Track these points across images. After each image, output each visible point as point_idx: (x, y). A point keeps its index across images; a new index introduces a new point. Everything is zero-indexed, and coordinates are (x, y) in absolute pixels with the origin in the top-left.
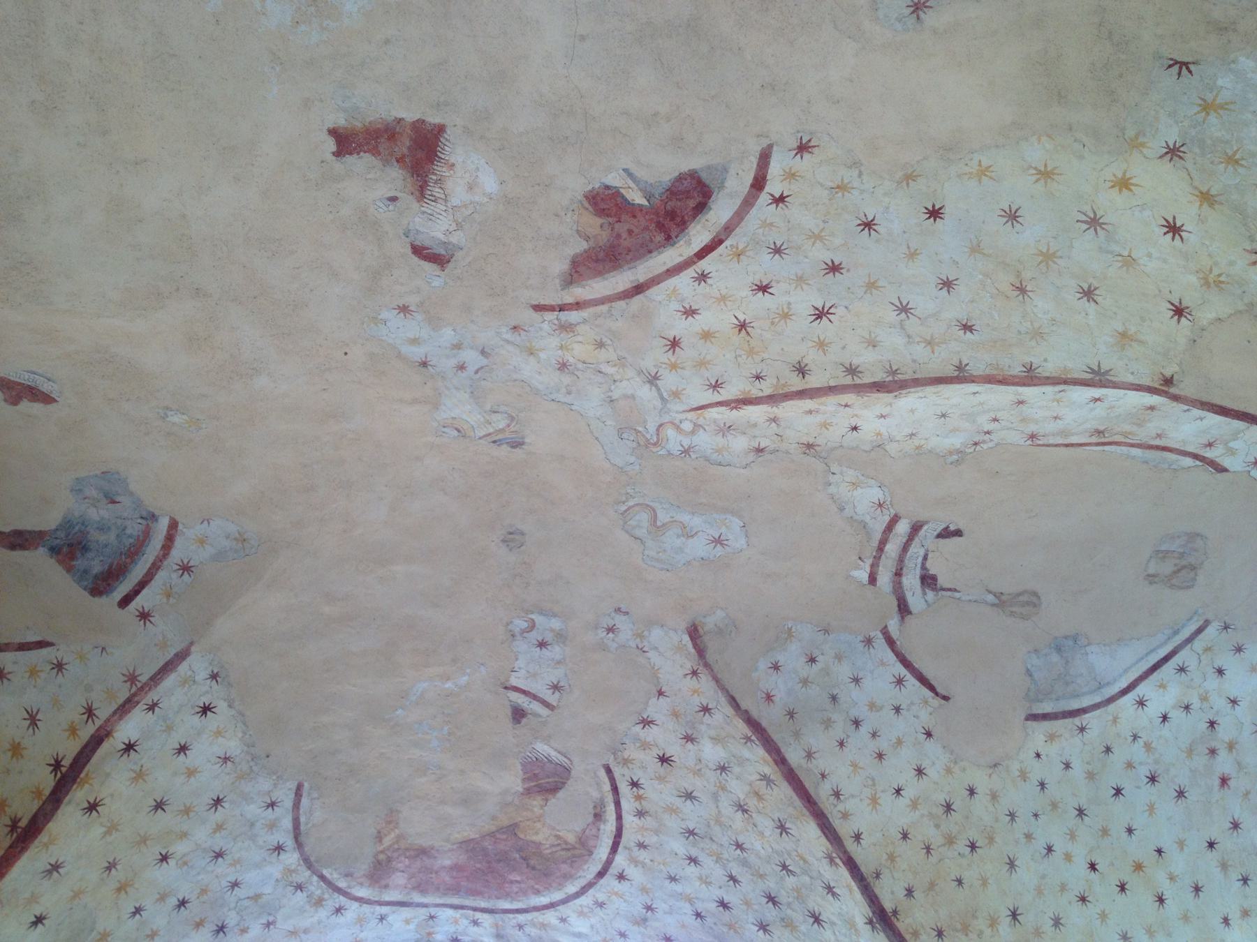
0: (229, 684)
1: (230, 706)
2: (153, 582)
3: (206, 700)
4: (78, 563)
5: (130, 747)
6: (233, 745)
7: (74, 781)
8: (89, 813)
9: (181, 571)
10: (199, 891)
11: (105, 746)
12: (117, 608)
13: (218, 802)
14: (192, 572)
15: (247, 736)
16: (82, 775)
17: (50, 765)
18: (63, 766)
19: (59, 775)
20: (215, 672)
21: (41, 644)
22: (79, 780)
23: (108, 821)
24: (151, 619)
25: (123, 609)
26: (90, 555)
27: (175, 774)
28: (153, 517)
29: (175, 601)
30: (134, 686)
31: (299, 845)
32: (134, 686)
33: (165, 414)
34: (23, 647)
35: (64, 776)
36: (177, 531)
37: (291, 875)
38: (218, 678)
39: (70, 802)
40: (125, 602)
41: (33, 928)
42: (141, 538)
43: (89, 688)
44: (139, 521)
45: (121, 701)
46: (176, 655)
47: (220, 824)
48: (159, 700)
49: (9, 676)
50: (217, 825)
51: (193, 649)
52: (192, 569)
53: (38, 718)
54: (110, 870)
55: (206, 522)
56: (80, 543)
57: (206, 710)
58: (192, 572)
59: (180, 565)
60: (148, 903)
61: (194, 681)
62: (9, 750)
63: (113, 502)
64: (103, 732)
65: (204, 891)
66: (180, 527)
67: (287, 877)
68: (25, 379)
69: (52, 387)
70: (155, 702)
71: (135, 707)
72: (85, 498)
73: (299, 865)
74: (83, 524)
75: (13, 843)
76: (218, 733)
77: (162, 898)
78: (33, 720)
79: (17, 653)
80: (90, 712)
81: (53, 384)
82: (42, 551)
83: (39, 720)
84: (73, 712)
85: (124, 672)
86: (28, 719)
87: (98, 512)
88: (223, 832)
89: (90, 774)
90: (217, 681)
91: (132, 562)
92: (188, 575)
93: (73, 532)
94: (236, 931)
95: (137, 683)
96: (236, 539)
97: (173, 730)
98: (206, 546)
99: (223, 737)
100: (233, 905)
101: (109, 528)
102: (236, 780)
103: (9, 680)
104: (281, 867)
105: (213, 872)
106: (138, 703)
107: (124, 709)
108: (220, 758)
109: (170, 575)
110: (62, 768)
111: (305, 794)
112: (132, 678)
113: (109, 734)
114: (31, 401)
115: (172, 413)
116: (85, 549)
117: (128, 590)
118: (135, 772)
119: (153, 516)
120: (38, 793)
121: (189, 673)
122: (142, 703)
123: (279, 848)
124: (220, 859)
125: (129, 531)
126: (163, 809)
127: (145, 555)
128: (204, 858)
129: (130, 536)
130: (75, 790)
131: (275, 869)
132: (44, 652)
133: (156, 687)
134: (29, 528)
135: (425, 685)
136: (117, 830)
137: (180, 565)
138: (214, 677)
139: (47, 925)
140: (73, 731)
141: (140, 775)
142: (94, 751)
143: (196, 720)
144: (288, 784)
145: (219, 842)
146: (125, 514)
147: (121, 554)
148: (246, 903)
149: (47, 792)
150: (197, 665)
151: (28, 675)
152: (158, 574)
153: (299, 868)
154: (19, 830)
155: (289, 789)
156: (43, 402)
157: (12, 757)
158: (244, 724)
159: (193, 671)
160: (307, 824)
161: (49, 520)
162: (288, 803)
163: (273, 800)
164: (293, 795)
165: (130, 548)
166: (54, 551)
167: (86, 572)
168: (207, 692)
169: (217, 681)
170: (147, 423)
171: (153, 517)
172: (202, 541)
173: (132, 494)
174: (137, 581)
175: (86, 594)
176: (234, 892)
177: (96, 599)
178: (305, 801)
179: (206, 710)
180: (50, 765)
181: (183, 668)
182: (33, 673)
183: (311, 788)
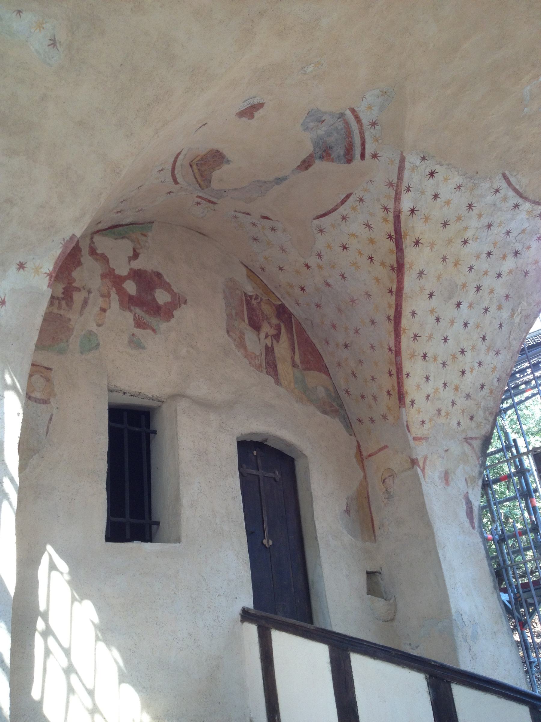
0: (433, 157)
1: (441, 165)
2: (366, 140)
3: (428, 170)
4: (333, 155)
5: (413, 211)
6: (458, 180)
7: (401, 238)
8: (417, 246)
9: (373, 127)
10: (492, 245)
11: (403, 217)
12: (363, 161)
13: (470, 206)
14: (377, 123)
15: (460, 172)
16: (403, 234)
17: (388, 238)
18: (392, 236)
19: (394, 240)
20: (422, 156)
21: (348, 196)
22: (403, 237)
23: (428, 243)
24: (378, 155)
25: (364, 160)
26: (335, 149)
27: (441, 208)
28: (342, 115)
29: (381, 140)
30: (394, 187)
31: (526, 199)
32: (394, 187)
33: (304, 71)
34: (343, 202)
35: (396, 239)
36: (356, 112)
37: (532, 213)
38: (426, 158)
39: (406, 247)
40: (363, 156)
41: (431, 299)
42: (346, 126)
43: (378, 200)
44: (339, 120)
45: (394, 196)
46: (400, 162)
47: (479, 214)
48: (408, 185)
49: (347, 216)
50: (478, 215)
51: (404, 154)
52: (377, 122)
53: (369, 224)
54: (445, 260)
55: (364, 99)
56: (327, 147)
57: (432, 174)
58: (377, 123)
59: (370, 125)
60: (473, 262)
61: (417, 167)
62: (369, 243)
63: (323, 122)
64: (397, 213)
65: (495, 244)
66: (356, 109)
67: (531, 214)
68: (246, 105)
69: (257, 99)
70: (407, 187)
71: (401, 194)
72: (312, 129)
73: (533, 206)
74: (321, 139)
75: (397, 274)
76: (446, 180)
77: (478, 257)
78: (368, 226)
79: (343, 206)
80: (386, 209)
81: (257, 98)
82: (317, 162)
83: (371, 225)
84: (381, 213)
85: (386, 184)
86: (367, 227)
87: (322, 130)
88: (484, 216)
89: (405, 231)
90: (426, 160)
91: (352, 139)
92: (377, 126)
93: (321, 145)
94: (524, 250)
95: (394, 185)
96: (382, 95)
97: (425, 192)
98: (373, 108)
99: (450, 179)
100: (514, 241)
101: (331, 133)
102: (471, 192)
103: (348, 218)
104: (524, 213)
105: (492, 234)
106: (401, 192)
107: (397, 198)
108: (456, 188)
109: (370, 131)
110: (393, 237)
111: (509, 176)
112: (391, 184)
113: (400, 212)
114: (256, 111)
115: (306, 68)
116: (331, 148)
117: (360, 151)
118: (423, 218)
119: (342, 114)
120: (391, 251)
121: (412, 165)
122: (402, 191)
123: (517, 206)
124: (492, 227)
125: (339, 128)
126: (448, 224)
127: (354, 132)
128: (483, 231)
129: (342, 129)
130: (404, 241)
131: (522, 215)
132: (351, 198)
133: (403, 181)
134: (305, 157)
135: (528, 88)
136: (435, 244)
137: (370, 125)
138: (423, 159)
139: (436, 295)
140: (386, 220)
141: (426, 219)
142: (399, 222)
143: (431, 181)
144: (497, 177)
145: (485, 221)
146: (332, 122)
147: (345, 139)
148: (520, 236)
149: (395, 249)
150: (412, 159)
151: (353, 211)
152: (365, 135)
153: (534, 207)
154: (396, 269)
155: (500, 179)
156: (261, 108)
157: (372, 244)
158: (454, 167)
159: (413, 163)
160: (521, 188)
161: (309, 148)
162: (504, 185)
163: (496, 189)
164: (504, 181)
165: (346, 134)
166: (321, 158)
167: (339, 157)
168: (426, 167)
169: (426, 160)
170: (302, 81)
171: (342, 115)
172: (370, 108)
173: (325, 113)
174: (360, 145)
175: (346, 165)
176: (511, 236)
177: (351, 164)
178: (512, 180)
179: (432, 174)
180: (388, 238)
181: (407, 165)
182: (354, 209)
183: (510, 172)
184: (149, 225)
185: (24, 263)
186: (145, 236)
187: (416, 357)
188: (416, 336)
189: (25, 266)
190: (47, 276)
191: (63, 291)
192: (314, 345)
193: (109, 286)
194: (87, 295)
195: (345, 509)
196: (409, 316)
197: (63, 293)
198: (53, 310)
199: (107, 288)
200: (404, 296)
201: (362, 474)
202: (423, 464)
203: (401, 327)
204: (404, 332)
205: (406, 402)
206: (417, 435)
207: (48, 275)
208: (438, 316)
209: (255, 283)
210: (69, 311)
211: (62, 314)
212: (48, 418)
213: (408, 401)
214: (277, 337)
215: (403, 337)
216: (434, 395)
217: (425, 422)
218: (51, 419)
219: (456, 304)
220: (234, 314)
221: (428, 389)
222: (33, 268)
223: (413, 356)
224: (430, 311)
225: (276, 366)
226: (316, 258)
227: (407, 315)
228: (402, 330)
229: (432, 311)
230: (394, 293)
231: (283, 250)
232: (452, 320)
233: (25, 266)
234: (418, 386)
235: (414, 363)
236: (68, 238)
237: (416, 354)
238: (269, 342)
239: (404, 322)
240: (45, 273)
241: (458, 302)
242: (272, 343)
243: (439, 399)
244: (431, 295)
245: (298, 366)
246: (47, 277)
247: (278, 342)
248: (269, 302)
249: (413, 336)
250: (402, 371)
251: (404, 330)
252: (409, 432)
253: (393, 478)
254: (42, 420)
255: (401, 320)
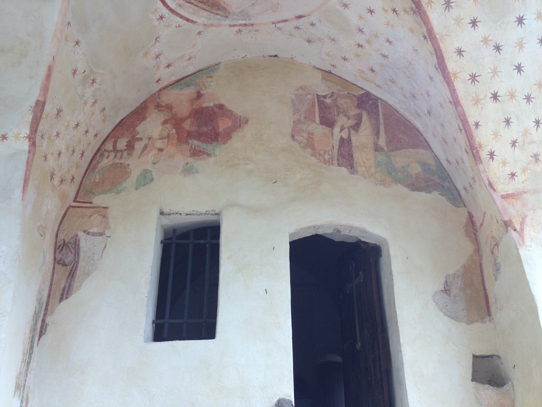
41: (476, 27)
184: (216, 67)
185: (5, 135)
186: (211, 77)
187: (482, 101)
188: (473, 78)
189: (6, 136)
190: (26, 139)
191: (126, 144)
192: (410, 122)
193: (169, 129)
194: (147, 142)
195: (443, 289)
196: (455, 56)
197: (127, 146)
198: (115, 161)
199: (168, 131)
200: (438, 36)
201: (470, 248)
202: (521, 225)
203: (449, 73)
204: (456, 77)
205: (481, 157)
206: (507, 191)
207: (27, 137)
208: (496, 44)
209: (332, 82)
210: (129, 158)
211: (122, 162)
212: (103, 246)
213: (484, 154)
214: (356, 127)
215: (455, 83)
216: (524, 139)
217: (516, 174)
218: (105, 247)
219: (517, 21)
220: (302, 119)
221: (513, 133)
222: (14, 136)
223: (477, 101)
224: (482, 41)
225: (352, 156)
226: (360, 34)
227: (452, 56)
228: (451, 75)
229: (485, 41)
230: (427, 37)
231: (333, 40)
232: (518, 42)
233: (6, 136)
234: (496, 135)
235: (482, 108)
236: (34, 104)
237: (481, 97)
238: (345, 135)
239: (452, 65)
240: (24, 137)
241: (517, 18)
242: (349, 134)
243: (532, 142)
244: (474, 23)
245: (383, 149)
246: (27, 140)
247: (357, 131)
248: (349, 96)
249: (470, 78)
250: (467, 122)
251: (455, 74)
252: (494, 190)
253: (498, 246)
254: (98, 249)
255: (446, 65)
